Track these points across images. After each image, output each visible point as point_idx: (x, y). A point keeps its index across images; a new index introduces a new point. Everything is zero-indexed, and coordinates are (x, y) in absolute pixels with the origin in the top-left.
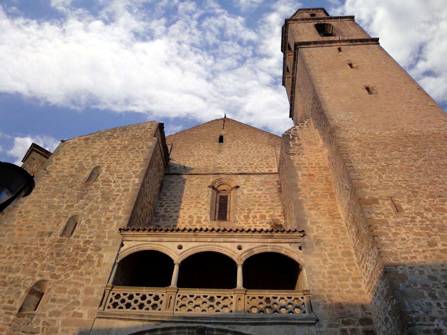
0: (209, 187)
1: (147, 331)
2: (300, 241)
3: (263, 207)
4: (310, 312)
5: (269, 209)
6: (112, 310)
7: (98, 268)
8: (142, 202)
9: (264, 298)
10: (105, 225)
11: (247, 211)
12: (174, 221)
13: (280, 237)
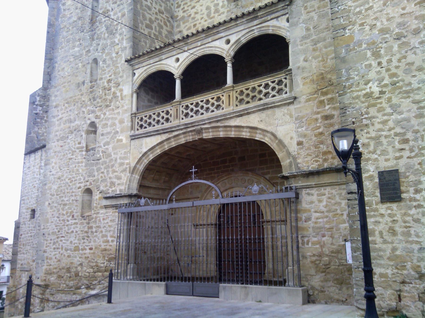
10: (117, 60)
12: (193, 21)
13: (265, 15)
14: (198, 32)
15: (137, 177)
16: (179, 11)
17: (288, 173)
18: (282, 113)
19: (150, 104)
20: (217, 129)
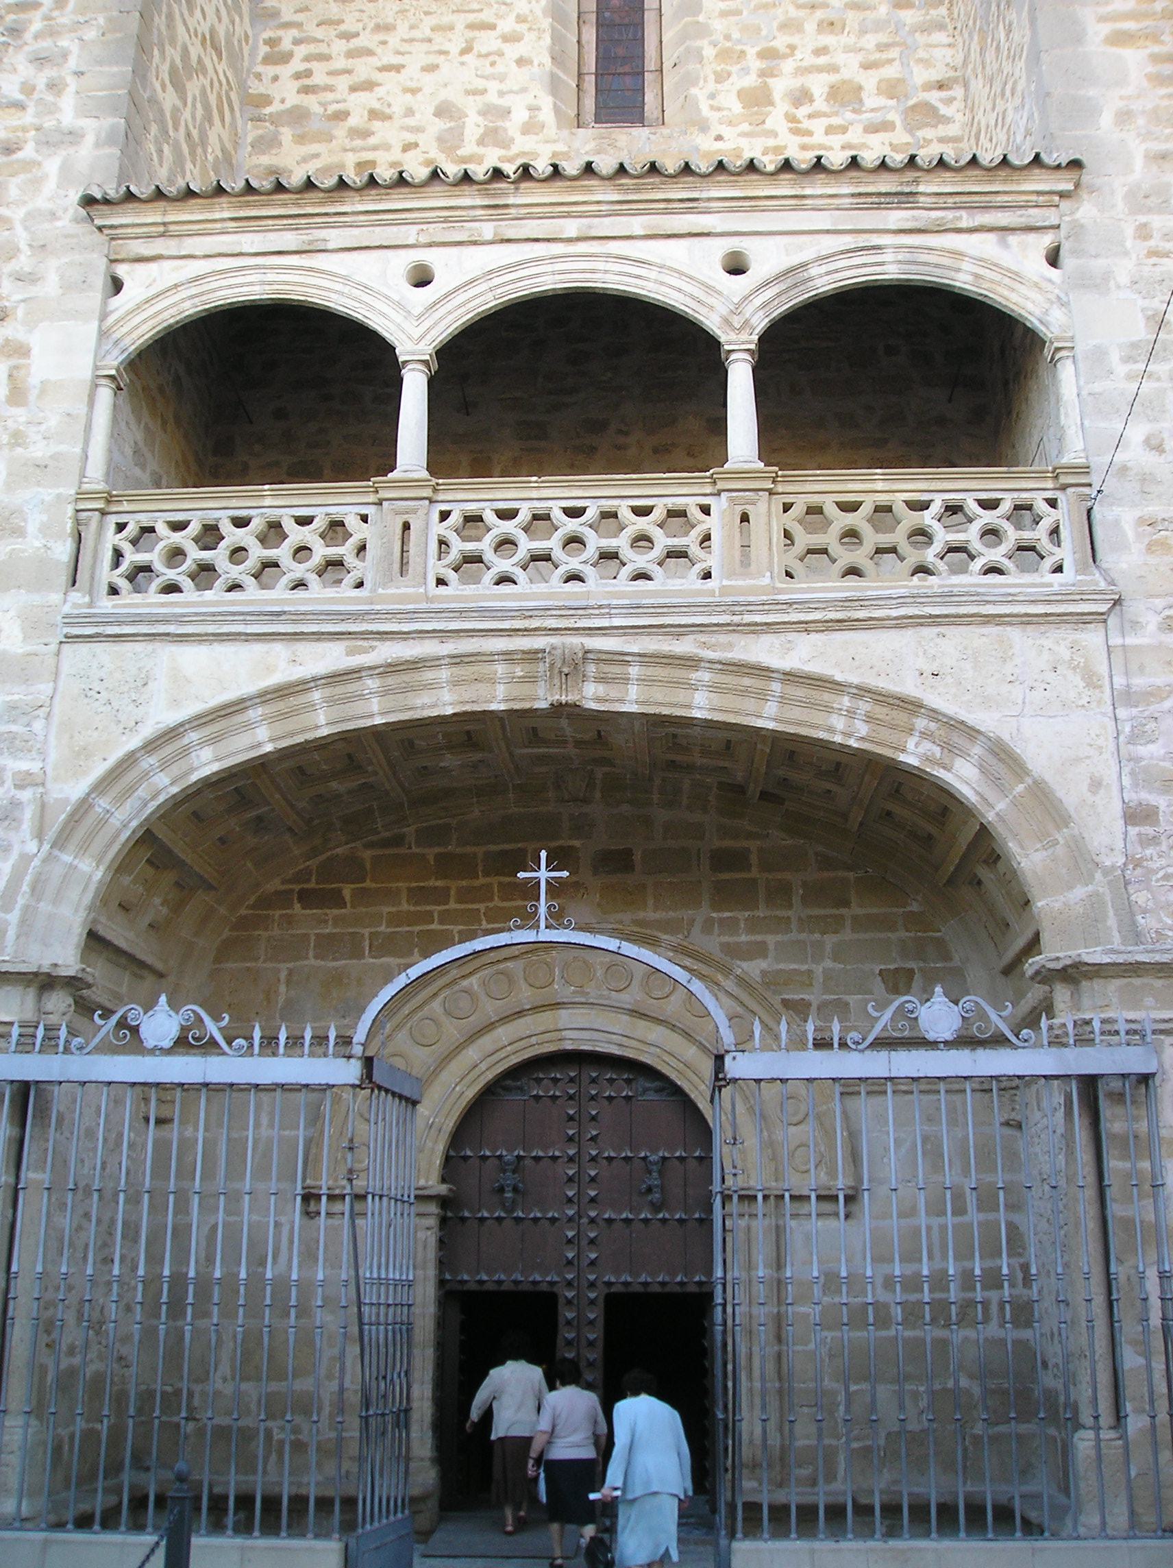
1: (314, 679)
2: (1051, 217)
3: (844, 39)
4: (1081, 569)
5: (881, 48)
6: (129, 601)
7: (15, 411)
8: (173, 42)
9: (866, 509)
11: (756, 64)
12: (358, 143)
13: (950, 200)
15: (90, 869)
16: (275, 78)
17: (1106, 952)
18: (1046, 655)
19: (137, 472)
20: (678, 673)
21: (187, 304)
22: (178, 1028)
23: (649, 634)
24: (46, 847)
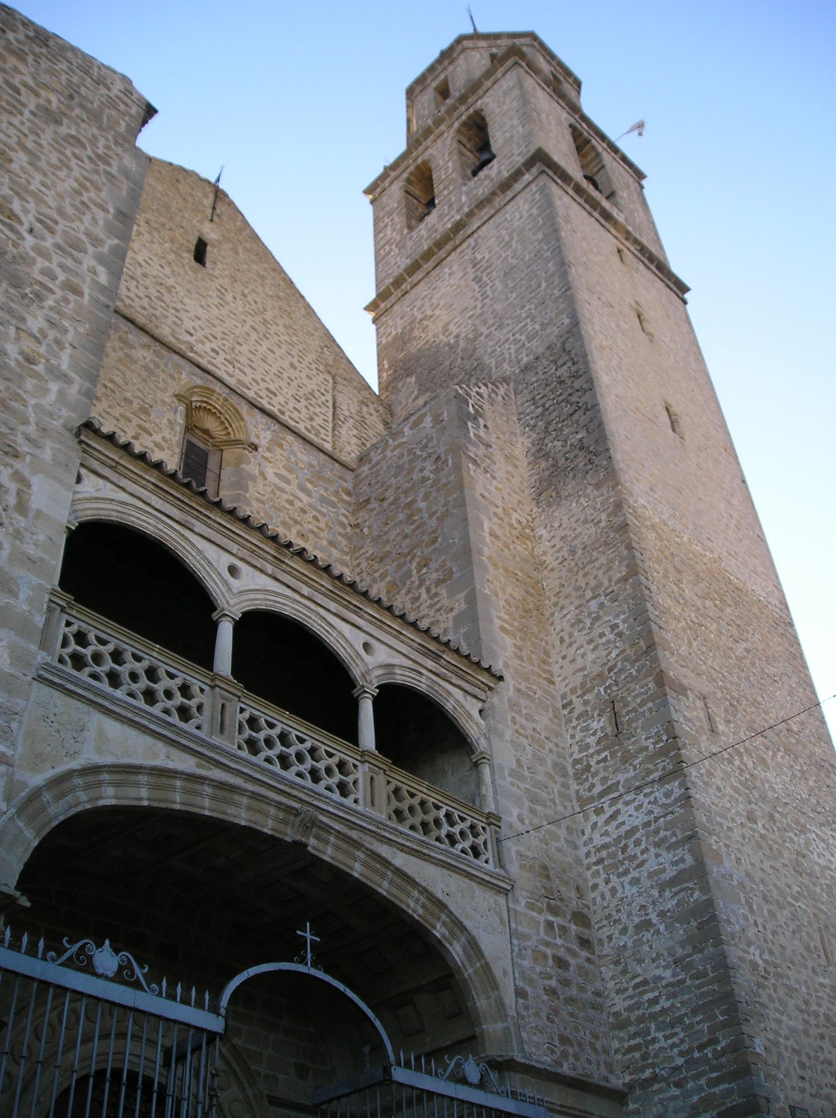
0: (178, 397)
1: (182, 773)
13: (452, 668)
14: (327, 569)
21: (114, 514)
22: (117, 965)
23: (340, 822)
24: (13, 810)
